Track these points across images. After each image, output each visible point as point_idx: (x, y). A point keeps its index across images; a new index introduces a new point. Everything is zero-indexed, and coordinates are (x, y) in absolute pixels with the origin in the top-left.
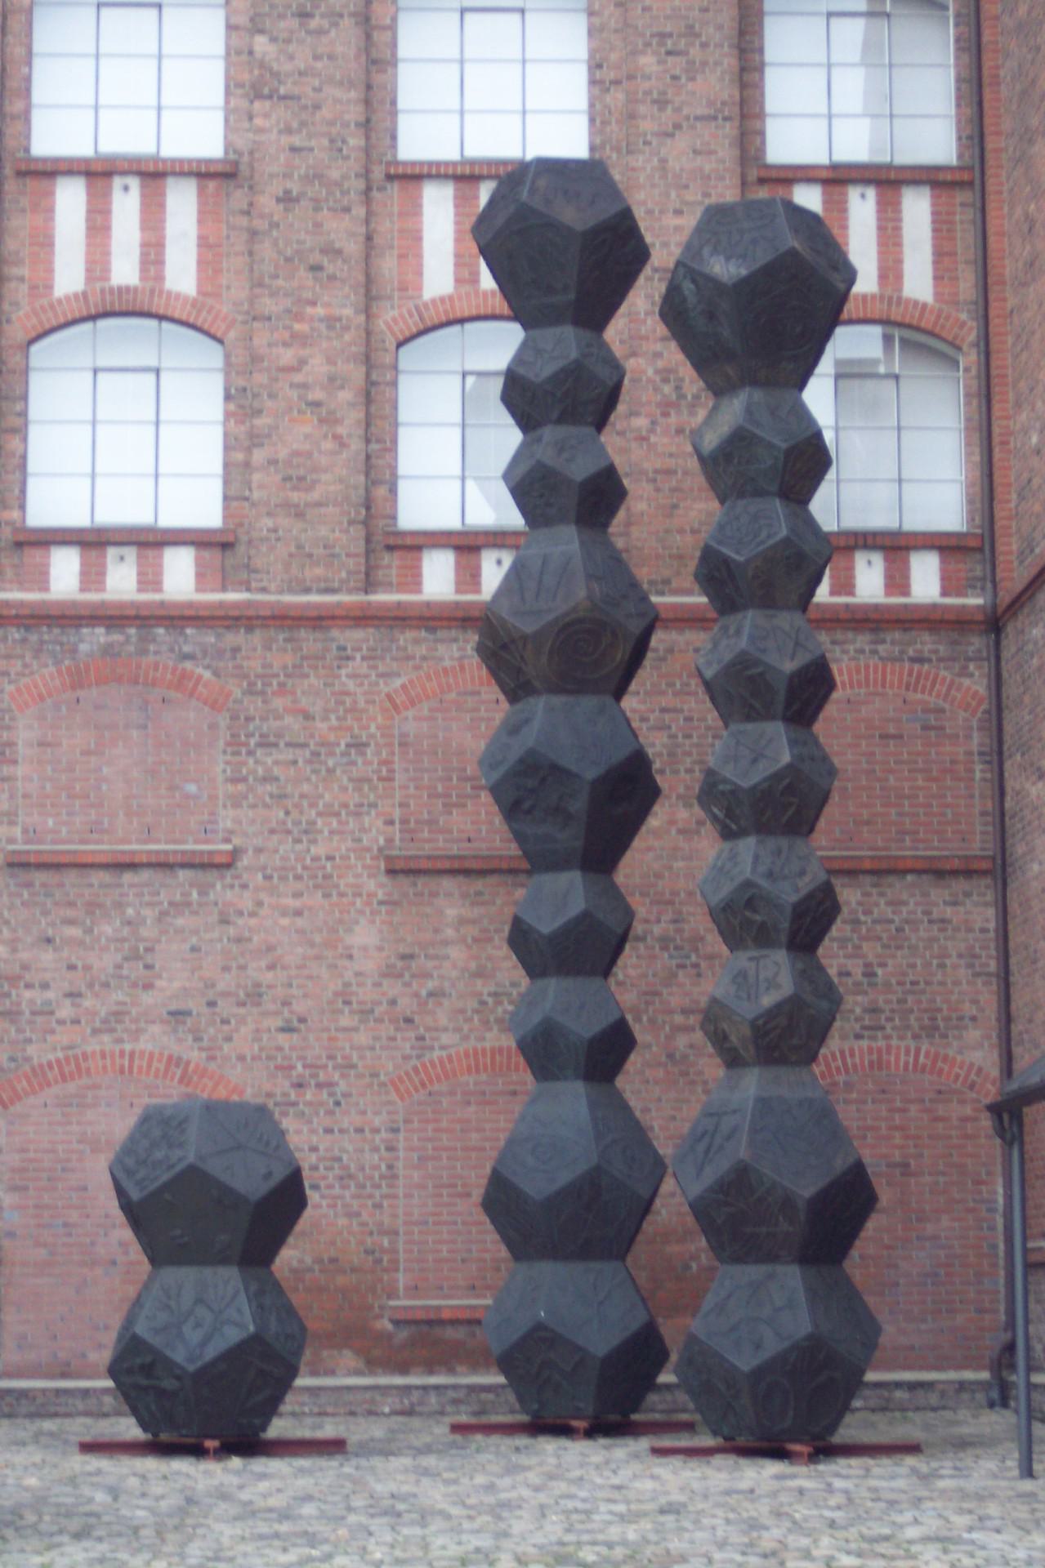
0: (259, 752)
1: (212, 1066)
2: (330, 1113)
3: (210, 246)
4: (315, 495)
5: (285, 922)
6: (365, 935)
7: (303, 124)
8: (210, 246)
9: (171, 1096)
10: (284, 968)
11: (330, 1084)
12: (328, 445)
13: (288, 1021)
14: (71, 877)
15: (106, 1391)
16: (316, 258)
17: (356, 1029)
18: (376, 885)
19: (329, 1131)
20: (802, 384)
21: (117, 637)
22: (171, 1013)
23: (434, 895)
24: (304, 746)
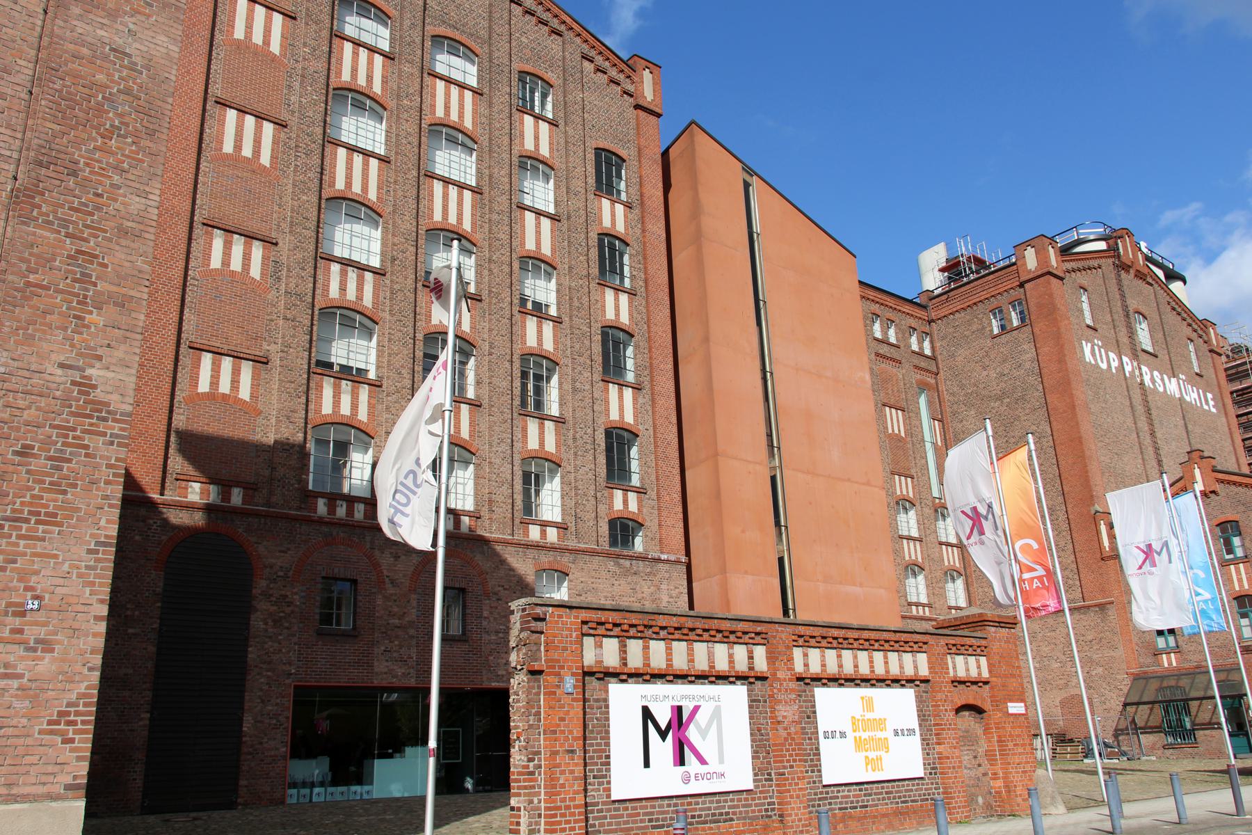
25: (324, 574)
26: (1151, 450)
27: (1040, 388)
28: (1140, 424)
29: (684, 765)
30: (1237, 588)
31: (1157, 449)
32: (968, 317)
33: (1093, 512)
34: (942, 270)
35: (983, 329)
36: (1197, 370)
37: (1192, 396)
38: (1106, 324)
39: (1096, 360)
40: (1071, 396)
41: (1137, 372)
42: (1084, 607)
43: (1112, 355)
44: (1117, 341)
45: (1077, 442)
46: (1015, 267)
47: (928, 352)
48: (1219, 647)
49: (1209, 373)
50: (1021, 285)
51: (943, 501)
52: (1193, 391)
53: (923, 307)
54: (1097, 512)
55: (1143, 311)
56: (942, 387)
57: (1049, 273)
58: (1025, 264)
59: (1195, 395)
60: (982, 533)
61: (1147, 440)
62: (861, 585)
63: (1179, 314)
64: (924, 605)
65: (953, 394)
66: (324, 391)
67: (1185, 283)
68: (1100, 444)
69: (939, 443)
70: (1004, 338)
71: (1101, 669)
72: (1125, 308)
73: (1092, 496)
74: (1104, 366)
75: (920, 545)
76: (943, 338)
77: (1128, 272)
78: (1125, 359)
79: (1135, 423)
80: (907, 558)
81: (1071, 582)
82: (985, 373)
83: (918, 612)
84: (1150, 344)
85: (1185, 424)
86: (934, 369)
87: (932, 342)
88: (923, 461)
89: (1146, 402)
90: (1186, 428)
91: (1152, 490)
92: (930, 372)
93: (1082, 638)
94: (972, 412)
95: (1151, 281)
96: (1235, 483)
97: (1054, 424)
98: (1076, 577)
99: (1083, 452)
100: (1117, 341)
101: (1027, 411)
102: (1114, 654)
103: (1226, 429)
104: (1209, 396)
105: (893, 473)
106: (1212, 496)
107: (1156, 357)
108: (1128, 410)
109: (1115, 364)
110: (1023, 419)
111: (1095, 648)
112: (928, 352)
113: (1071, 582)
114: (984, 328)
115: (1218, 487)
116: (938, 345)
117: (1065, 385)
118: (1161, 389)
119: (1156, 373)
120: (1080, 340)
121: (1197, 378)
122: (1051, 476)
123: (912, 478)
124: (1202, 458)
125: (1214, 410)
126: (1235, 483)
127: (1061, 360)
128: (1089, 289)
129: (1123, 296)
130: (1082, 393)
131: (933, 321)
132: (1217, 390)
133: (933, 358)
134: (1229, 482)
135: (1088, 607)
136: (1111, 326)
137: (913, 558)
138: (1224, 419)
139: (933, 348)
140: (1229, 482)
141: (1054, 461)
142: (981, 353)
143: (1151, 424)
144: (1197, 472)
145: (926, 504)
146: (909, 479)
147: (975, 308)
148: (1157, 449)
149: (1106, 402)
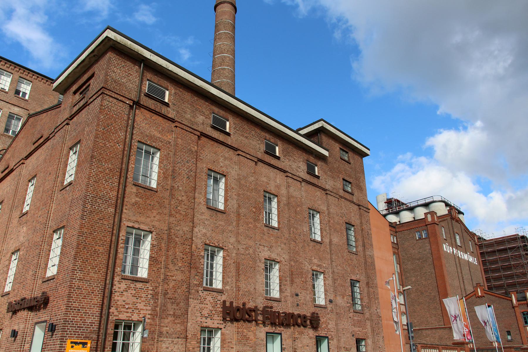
26: (461, 278)
27: (432, 258)
28: (458, 270)
31: (463, 278)
32: (409, 233)
34: (385, 203)
35: (414, 237)
36: (472, 251)
37: (471, 260)
38: (449, 238)
39: (447, 250)
40: (441, 262)
41: (457, 253)
42: (444, 327)
43: (451, 248)
44: (452, 243)
45: (443, 276)
46: (424, 220)
47: (395, 242)
48: (485, 342)
49: (475, 252)
50: (426, 225)
53: (394, 227)
55: (458, 232)
56: (400, 254)
57: (435, 223)
58: (427, 219)
59: (472, 259)
60: (456, 321)
61: (460, 275)
63: (467, 232)
65: (403, 256)
67: (463, 215)
68: (449, 277)
70: (420, 241)
72: (453, 232)
73: (447, 294)
74: (449, 252)
76: (400, 238)
77: (454, 220)
78: (454, 249)
79: (457, 270)
81: (440, 319)
82: (414, 251)
84: (460, 243)
85: (470, 269)
86: (397, 248)
87: (397, 239)
89: (460, 263)
90: (470, 270)
91: (483, 307)
92: (396, 248)
94: (410, 263)
95: (459, 222)
96: (490, 294)
97: (436, 270)
98: (442, 318)
99: (445, 280)
100: (452, 243)
101: (427, 265)
103: (480, 270)
104: (475, 259)
106: (483, 297)
107: (461, 247)
108: (455, 265)
109: (451, 251)
110: (426, 267)
112: (395, 242)
113: (440, 319)
114: (414, 237)
115: (485, 295)
116: (398, 240)
117: (439, 258)
118: (463, 258)
119: (462, 253)
120: (443, 244)
121: (472, 253)
122: (435, 286)
124: (480, 286)
125: (477, 264)
126: (490, 294)
127: (438, 251)
128: (444, 227)
129: (453, 228)
130: (444, 261)
131: (397, 232)
132: (477, 257)
133: (397, 244)
134: (488, 294)
135: (446, 328)
136: (450, 238)
138: (479, 267)
139: (397, 241)
140: (488, 294)
141: (436, 281)
142: (413, 245)
143: (461, 270)
144: (479, 290)
147: (411, 230)
148: (463, 278)
149: (449, 263)
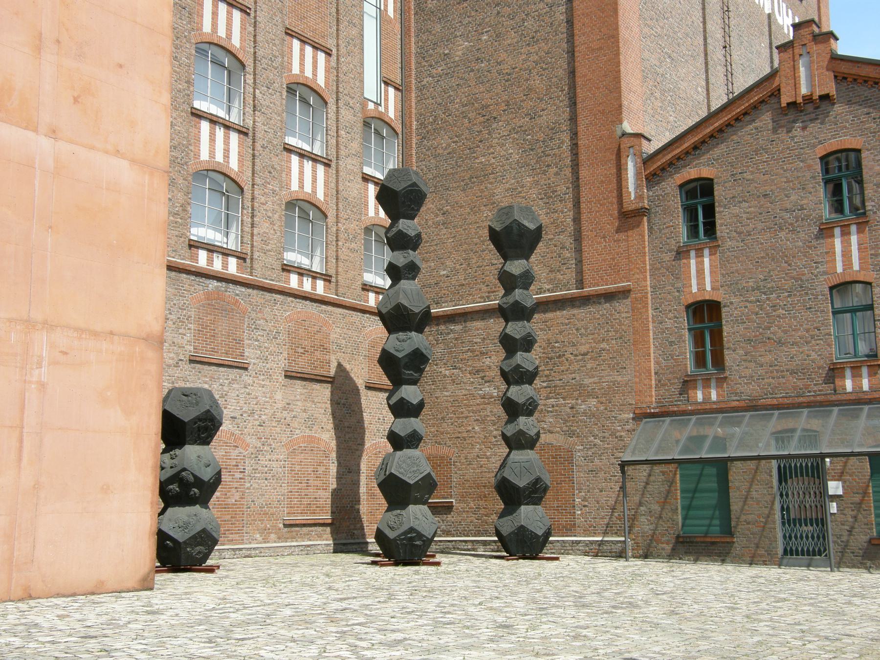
0: (255, 331)
1: (242, 436)
2: (270, 454)
3: (241, 156)
4: (269, 248)
5: (260, 389)
6: (279, 396)
7: (267, 124)
8: (241, 156)
9: (633, 469)
10: (260, 405)
11: (271, 445)
12: (272, 232)
13: (260, 423)
14: (206, 367)
15: (494, 541)
16: (270, 169)
17: (276, 427)
18: (281, 378)
19: (270, 460)
20: (513, 275)
21: (219, 284)
22: (231, 417)
23: (295, 385)
24: (266, 330)
25: (246, 377)
29: (538, 480)
30: (839, 269)
33: (619, 133)
51: (382, 109)
52: (787, 15)
54: (624, 134)
61: (717, 55)
62: (53, 133)
64: (314, 276)
66: (214, 263)
69: (391, 12)
71: (431, 79)
75: (326, 172)
80: (295, 186)
83: (314, 287)
88: (354, 32)
93: (570, 350)
102: (619, 379)
105: (290, 33)
111: (589, 366)
123: (328, 54)
137: (308, 188)
145: (347, 104)
146: (321, 56)
